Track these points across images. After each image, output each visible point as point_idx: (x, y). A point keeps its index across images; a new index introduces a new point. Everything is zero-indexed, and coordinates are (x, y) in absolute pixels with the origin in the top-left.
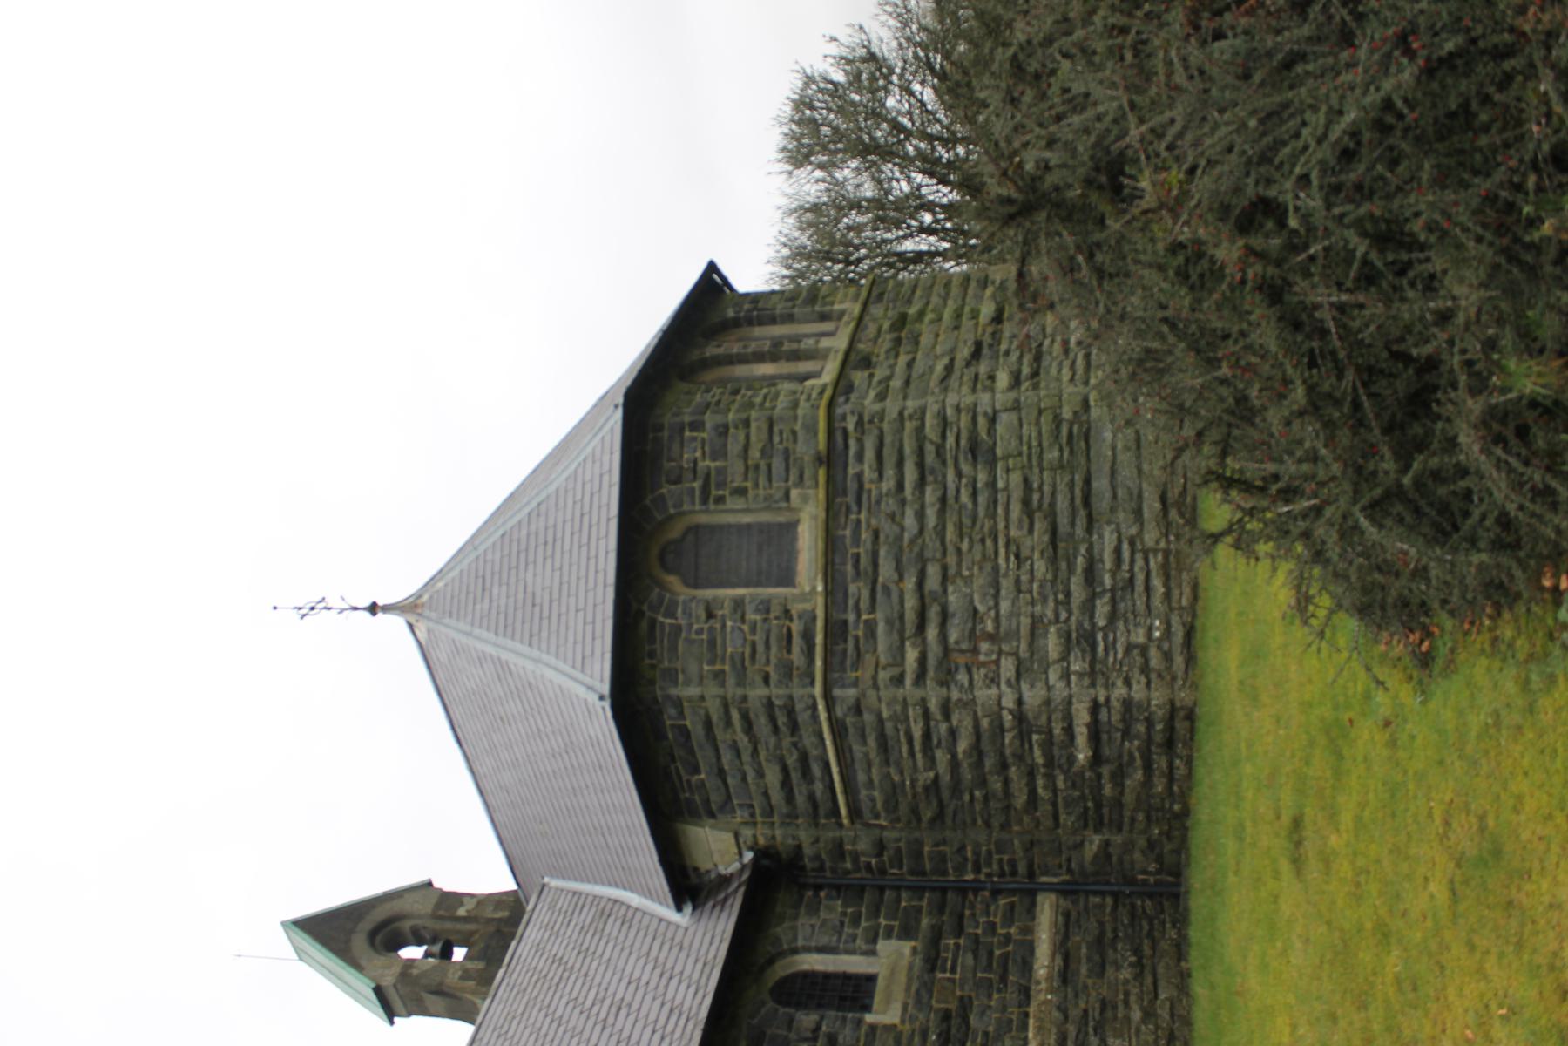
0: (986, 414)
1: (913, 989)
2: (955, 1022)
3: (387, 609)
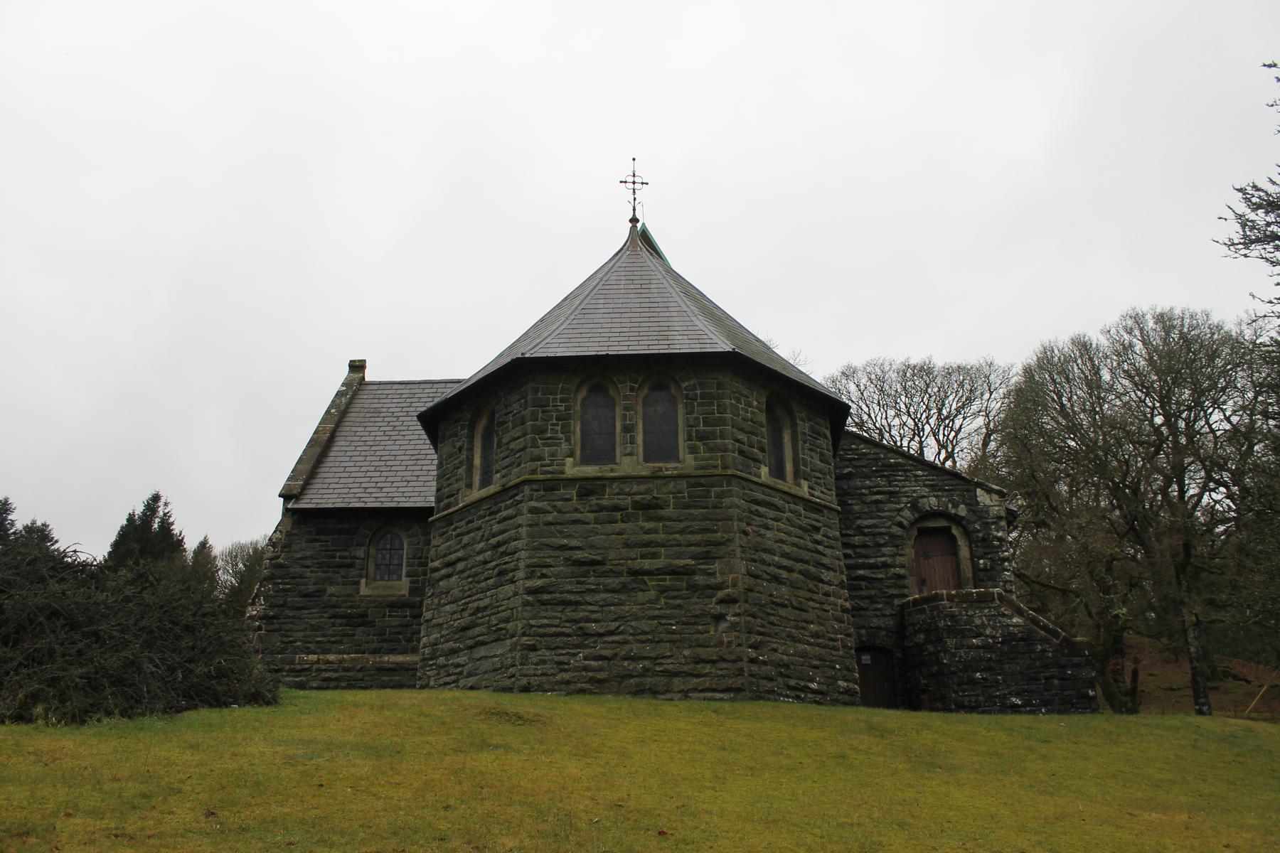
0: (514, 577)
1: (379, 599)
2: (360, 620)
3: (634, 213)
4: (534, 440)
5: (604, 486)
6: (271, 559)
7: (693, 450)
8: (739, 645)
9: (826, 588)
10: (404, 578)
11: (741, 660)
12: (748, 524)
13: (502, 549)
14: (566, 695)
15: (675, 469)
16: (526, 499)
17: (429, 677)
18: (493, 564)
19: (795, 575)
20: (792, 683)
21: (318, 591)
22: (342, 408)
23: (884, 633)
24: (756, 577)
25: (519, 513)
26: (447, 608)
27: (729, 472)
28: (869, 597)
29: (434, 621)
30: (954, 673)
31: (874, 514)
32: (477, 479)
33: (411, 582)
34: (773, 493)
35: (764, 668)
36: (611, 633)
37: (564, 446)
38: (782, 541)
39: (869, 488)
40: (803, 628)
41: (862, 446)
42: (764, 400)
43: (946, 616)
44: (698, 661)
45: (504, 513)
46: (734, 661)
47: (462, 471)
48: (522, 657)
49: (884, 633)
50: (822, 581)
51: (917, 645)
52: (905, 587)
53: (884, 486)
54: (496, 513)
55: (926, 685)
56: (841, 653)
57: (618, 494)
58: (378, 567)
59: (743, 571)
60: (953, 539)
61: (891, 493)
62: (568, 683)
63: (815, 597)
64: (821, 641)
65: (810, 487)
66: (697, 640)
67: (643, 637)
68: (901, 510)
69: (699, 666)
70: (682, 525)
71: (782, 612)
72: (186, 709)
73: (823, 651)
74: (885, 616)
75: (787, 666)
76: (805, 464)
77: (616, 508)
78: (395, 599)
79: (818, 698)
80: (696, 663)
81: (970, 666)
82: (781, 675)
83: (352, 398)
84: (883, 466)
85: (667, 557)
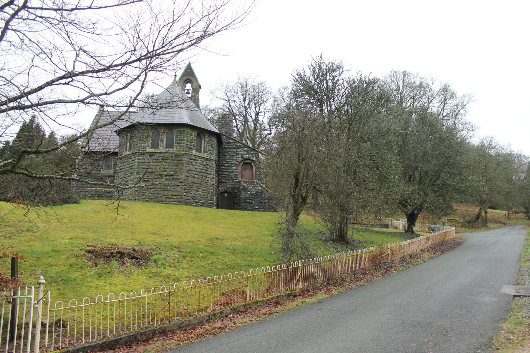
2: (101, 180)
4: (140, 142)
7: (176, 147)
9: (208, 179)
12: (188, 164)
13: (132, 167)
15: (172, 151)
19: (199, 176)
20: (195, 201)
22: (97, 120)
25: (135, 160)
28: (228, 180)
33: (114, 171)
34: (196, 156)
35: (188, 197)
36: (154, 188)
37: (147, 144)
44: (173, 195)
45: (133, 159)
46: (180, 196)
47: (124, 147)
50: (207, 177)
58: (106, 166)
59: (185, 175)
60: (252, 166)
61: (237, 153)
62: (144, 199)
63: (205, 181)
68: (239, 158)
70: (172, 164)
71: (195, 185)
73: (205, 194)
74: (231, 184)
75: (194, 197)
77: (157, 160)
79: (202, 204)
81: (246, 198)
82: (192, 199)
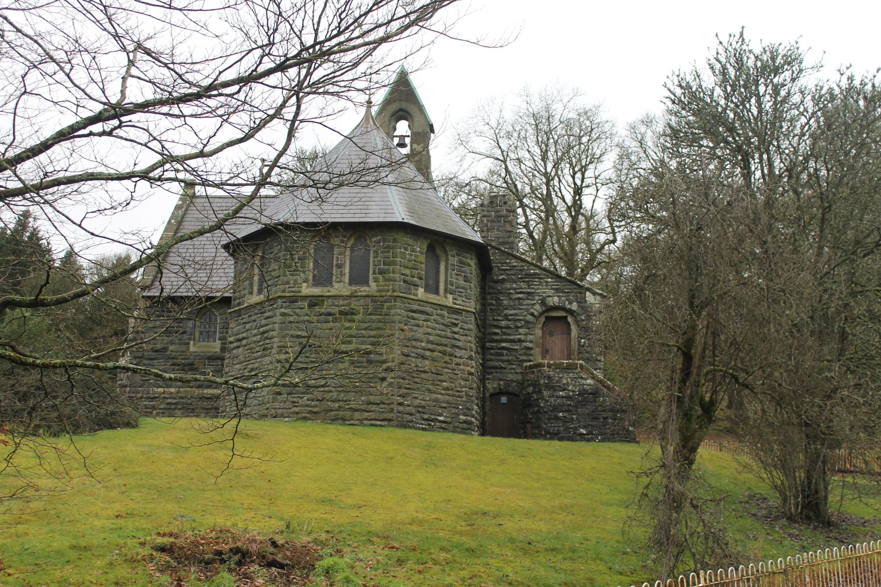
1: (202, 354)
5: (324, 300)
6: (133, 328)
7: (376, 280)
8: (392, 395)
9: (458, 360)
10: (217, 341)
11: (393, 403)
12: (406, 325)
13: (266, 335)
14: (296, 421)
16: (279, 307)
17: (226, 406)
18: (261, 343)
19: (435, 354)
20: (426, 416)
21: (164, 348)
22: (179, 219)
23: (515, 384)
24: (407, 356)
26: (237, 366)
27: (395, 294)
28: (508, 361)
29: (230, 374)
30: (546, 412)
31: (516, 307)
32: (255, 288)
35: (408, 408)
36: (323, 386)
38: (429, 334)
39: (515, 289)
40: (438, 385)
41: (513, 261)
42: (425, 247)
43: (545, 377)
44: (369, 403)
45: (268, 314)
48: (273, 398)
49: (515, 384)
50: (456, 357)
51: (528, 393)
52: (531, 355)
53: (525, 288)
54: (264, 313)
55: (531, 419)
56: (464, 399)
57: (331, 306)
58: (201, 333)
59: (399, 352)
61: (529, 293)
62: (297, 413)
63: (449, 366)
64: (450, 392)
65: (454, 299)
66: (369, 391)
67: (340, 389)
68: (534, 304)
69: (369, 406)
70: (366, 325)
71: (424, 376)
72: (98, 430)
73: (451, 398)
74: (517, 373)
75: (424, 407)
76: (452, 284)
77: (329, 314)
78: (211, 354)
79: (443, 425)
80: (368, 404)
81: (556, 409)
82: (419, 412)
83: (186, 210)
84: (526, 275)
85: (356, 343)
